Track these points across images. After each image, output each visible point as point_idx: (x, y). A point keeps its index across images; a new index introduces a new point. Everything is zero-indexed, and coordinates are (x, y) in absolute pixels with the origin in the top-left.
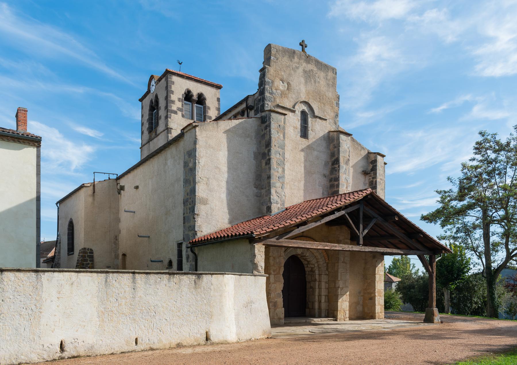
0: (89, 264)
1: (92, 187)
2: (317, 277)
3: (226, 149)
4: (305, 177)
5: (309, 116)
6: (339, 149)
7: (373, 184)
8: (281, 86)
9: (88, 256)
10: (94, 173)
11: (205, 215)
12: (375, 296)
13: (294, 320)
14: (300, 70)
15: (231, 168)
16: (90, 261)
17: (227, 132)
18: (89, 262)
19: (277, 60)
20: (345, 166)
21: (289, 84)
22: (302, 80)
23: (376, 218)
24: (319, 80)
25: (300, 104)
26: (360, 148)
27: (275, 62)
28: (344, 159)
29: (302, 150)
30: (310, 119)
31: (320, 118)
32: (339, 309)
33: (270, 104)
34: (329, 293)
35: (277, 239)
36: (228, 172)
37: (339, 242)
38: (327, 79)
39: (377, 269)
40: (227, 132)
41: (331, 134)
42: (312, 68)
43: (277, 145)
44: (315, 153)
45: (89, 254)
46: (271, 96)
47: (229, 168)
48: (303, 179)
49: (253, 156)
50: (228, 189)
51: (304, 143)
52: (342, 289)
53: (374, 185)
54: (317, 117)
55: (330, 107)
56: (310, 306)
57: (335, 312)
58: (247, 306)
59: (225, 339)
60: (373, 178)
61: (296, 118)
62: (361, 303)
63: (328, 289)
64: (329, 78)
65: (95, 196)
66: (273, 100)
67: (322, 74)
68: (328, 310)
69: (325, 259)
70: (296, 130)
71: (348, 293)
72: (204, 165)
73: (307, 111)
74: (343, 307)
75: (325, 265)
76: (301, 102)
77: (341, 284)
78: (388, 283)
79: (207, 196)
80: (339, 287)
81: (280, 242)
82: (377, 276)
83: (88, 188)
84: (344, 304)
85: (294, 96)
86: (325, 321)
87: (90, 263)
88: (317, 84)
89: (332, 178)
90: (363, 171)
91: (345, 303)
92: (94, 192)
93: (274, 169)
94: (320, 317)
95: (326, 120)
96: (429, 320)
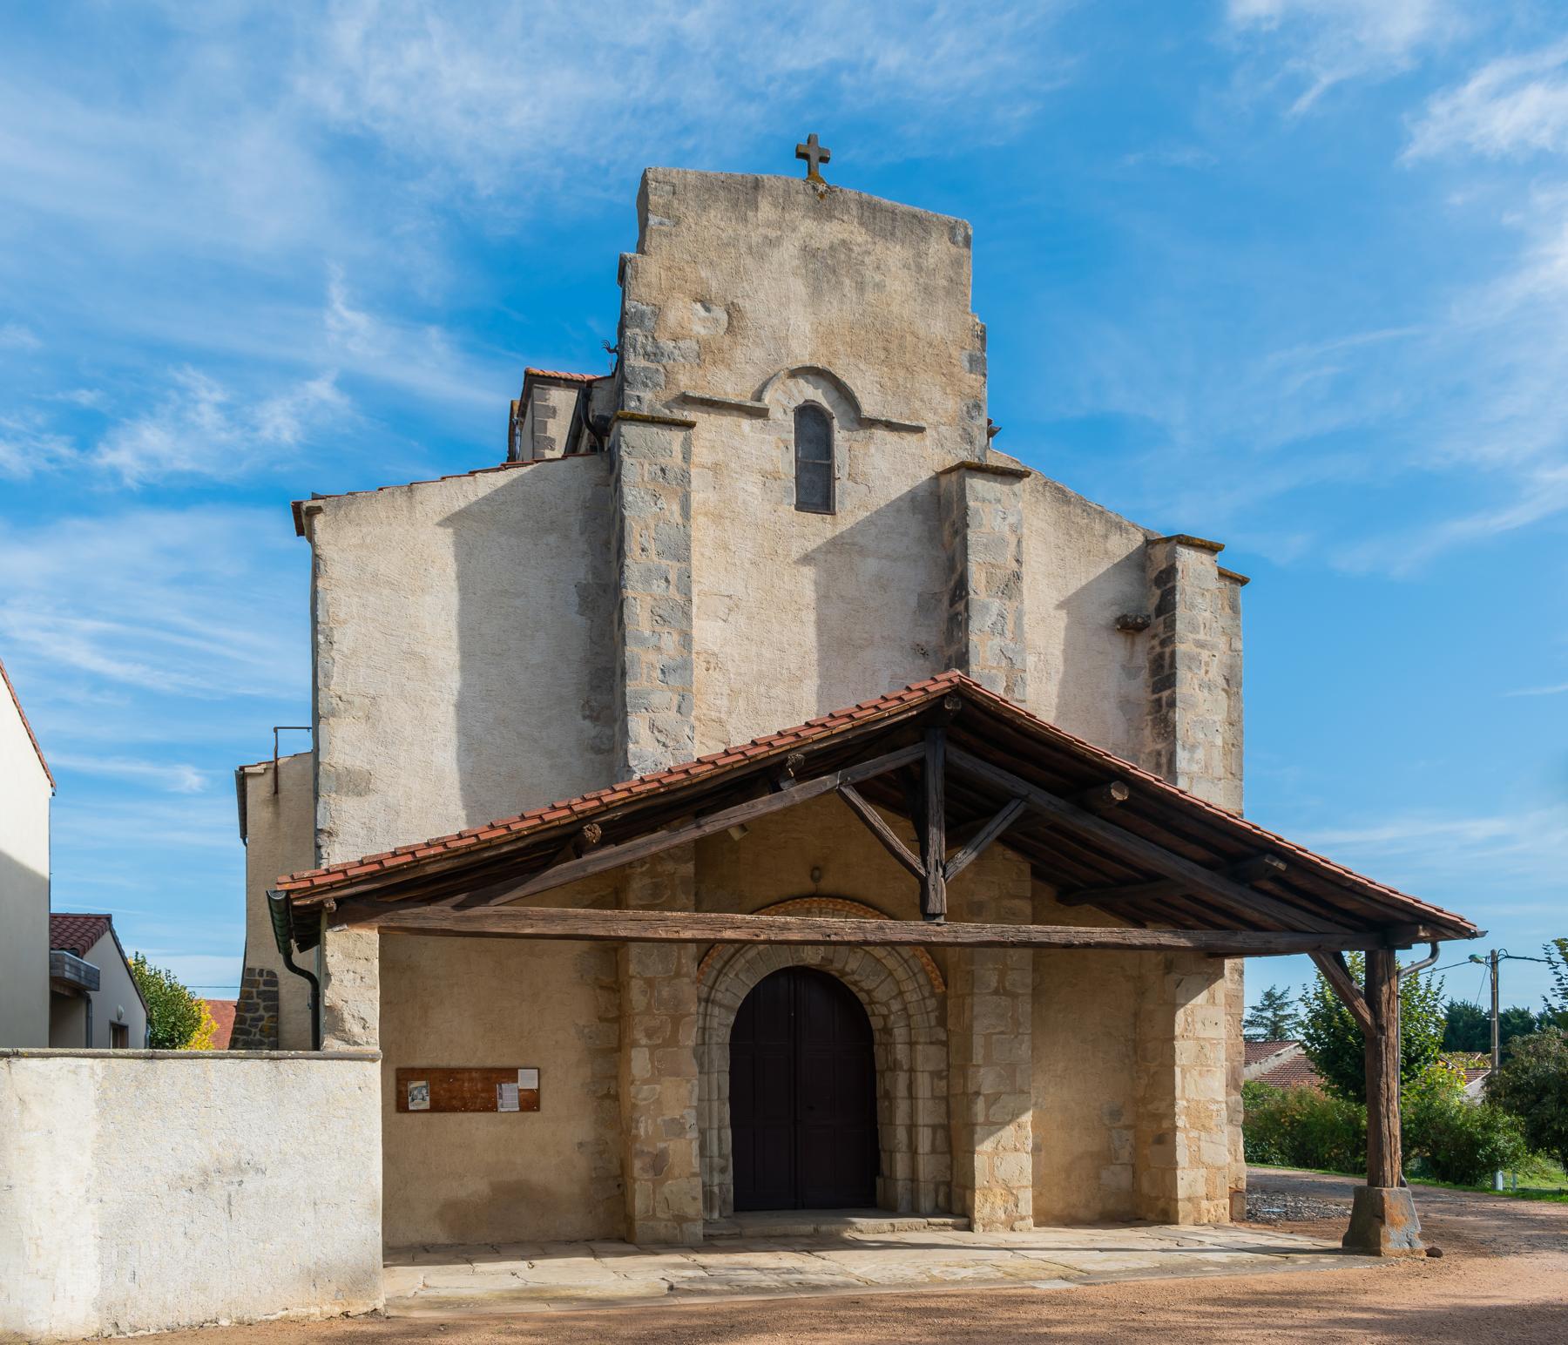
0: (261, 1019)
1: (270, 776)
2: (901, 1052)
3: (454, 584)
4: (821, 662)
5: (835, 422)
6: (965, 538)
7: (1162, 666)
8: (686, 317)
9: (259, 993)
10: (276, 730)
11: (363, 833)
12: (1175, 1128)
14: (788, 251)
15: (475, 648)
16: (266, 1009)
17: (453, 520)
18: (261, 1012)
19: (677, 223)
20: (996, 605)
21: (733, 311)
22: (799, 288)
23: (1023, 798)
24: (878, 278)
25: (790, 383)
26: (1099, 527)
27: (668, 235)
28: (990, 576)
29: (806, 559)
30: (840, 436)
31: (890, 426)
32: (980, 1180)
33: (647, 395)
34: (949, 1114)
36: (463, 668)
38: (920, 268)
39: (1180, 1015)
40: (453, 520)
41: (944, 480)
42: (846, 236)
43: (652, 548)
44: (871, 565)
45: (262, 988)
47: (466, 654)
48: (813, 671)
49: (575, 599)
50: (464, 732)
51: (817, 530)
52: (992, 1100)
53: (1167, 671)
56: (886, 1173)
57: (968, 1192)
58: (204, 1185)
59: (14, 1326)
60: (1163, 643)
61: (772, 438)
62: (1125, 1154)
63: (946, 1099)
64: (931, 262)
65: (282, 803)
66: (662, 379)
67: (895, 254)
68: (949, 1184)
69: (930, 981)
70: (775, 485)
71: (1027, 1118)
72: (354, 652)
74: (1001, 1173)
75: (932, 1003)
76: (794, 374)
77: (986, 1079)
79: (370, 762)
80: (978, 1093)
81: (469, 919)
82: (1178, 1044)
83: (260, 779)
84: (1006, 1160)
85: (758, 354)
86: (911, 1229)
87: (266, 1015)
88: (870, 296)
89: (950, 658)
90: (1118, 620)
91: (1011, 1157)
92: (276, 792)
93: (641, 641)
94: (915, 1212)
96: (1362, 1238)
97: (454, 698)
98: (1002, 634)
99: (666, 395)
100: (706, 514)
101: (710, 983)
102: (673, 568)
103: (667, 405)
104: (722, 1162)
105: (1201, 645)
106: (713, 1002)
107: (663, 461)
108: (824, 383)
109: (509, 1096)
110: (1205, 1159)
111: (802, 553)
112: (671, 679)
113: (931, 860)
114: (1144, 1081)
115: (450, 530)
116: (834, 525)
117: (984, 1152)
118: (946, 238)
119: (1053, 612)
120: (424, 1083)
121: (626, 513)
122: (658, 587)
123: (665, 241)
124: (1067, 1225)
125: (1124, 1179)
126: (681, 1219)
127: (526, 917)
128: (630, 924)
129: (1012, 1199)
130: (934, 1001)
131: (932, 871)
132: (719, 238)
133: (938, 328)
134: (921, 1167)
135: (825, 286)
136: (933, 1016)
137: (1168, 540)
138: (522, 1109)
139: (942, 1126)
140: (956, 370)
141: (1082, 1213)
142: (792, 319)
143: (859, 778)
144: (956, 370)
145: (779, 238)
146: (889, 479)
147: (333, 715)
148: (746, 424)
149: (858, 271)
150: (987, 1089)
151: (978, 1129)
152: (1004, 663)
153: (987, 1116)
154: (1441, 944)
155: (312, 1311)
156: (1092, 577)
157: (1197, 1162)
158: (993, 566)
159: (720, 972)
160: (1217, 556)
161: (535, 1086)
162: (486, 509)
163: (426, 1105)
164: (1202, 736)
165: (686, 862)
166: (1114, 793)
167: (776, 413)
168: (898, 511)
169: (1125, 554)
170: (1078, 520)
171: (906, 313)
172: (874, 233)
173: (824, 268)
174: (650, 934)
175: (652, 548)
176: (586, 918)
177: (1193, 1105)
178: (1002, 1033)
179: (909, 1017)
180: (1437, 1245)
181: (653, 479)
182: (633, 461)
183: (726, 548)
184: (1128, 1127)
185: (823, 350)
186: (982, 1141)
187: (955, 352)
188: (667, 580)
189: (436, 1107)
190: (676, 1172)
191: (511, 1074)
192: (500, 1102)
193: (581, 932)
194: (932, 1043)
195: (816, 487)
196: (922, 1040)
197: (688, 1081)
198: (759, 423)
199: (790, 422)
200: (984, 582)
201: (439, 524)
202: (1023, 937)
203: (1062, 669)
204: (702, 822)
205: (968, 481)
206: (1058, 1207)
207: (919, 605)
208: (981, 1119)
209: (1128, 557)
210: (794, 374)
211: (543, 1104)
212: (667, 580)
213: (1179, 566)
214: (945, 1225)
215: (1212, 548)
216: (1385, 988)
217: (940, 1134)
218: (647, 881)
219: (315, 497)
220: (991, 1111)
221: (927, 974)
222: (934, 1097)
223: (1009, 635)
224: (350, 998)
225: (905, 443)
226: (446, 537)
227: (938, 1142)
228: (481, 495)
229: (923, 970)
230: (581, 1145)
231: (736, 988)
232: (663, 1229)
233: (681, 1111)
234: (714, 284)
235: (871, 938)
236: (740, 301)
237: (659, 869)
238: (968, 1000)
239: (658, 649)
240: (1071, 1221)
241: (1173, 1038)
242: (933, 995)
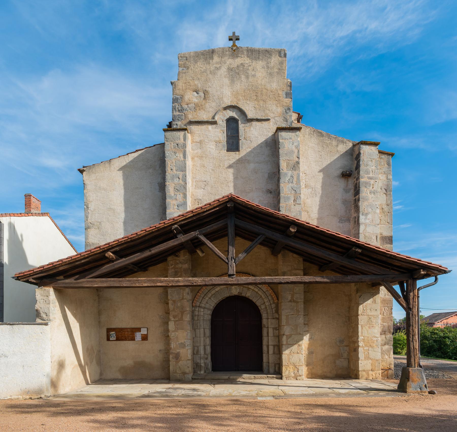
3: (122, 187)
5: (240, 122)
7: (356, 187)
12: (359, 346)
13: (225, 376)
20: (290, 173)
21: (206, 93)
22: (226, 81)
25: (224, 112)
27: (185, 73)
29: (230, 167)
31: (258, 120)
35: (76, 279)
37: (284, 274)
38: (268, 67)
39: (361, 307)
42: (242, 62)
43: (174, 169)
44: (252, 166)
46: (181, 114)
49: (157, 187)
51: (234, 156)
52: (289, 337)
54: (252, 120)
55: (275, 102)
62: (345, 355)
66: (183, 117)
67: (259, 65)
69: (273, 299)
72: (94, 210)
73: (236, 117)
75: (273, 306)
76: (225, 109)
77: (286, 330)
78: (200, 325)
79: (99, 241)
80: (284, 335)
81: (78, 283)
82: (359, 317)
84: (297, 355)
85: (214, 104)
86: (261, 378)
88: (251, 79)
93: (171, 197)
95: (268, 120)
97: (123, 220)
98: (292, 182)
99: (185, 122)
100: (197, 157)
101: (200, 301)
102: (181, 174)
103: (185, 125)
104: (206, 356)
105: (371, 178)
106: (201, 307)
107: (177, 142)
108: (235, 110)
109: (138, 336)
110: (371, 357)
111: (228, 165)
112: (180, 208)
113: (230, 257)
114: (351, 330)
115: (121, 172)
116: (239, 154)
117: (286, 354)
118: (277, 56)
119: (317, 174)
120: (114, 332)
121: (166, 159)
122: (176, 181)
123: (184, 75)
124: (323, 379)
125: (345, 364)
126: (184, 373)
127: (95, 281)
128: (127, 282)
129: (296, 369)
130: (274, 305)
131: (230, 260)
132: (201, 70)
133: (274, 86)
134: (270, 359)
135: (235, 79)
136: (274, 310)
137: (358, 143)
138: (142, 340)
139: (277, 345)
140: (281, 98)
141: (329, 375)
142: (224, 91)
143: (204, 232)
144: (281, 98)
145: (220, 67)
146: (258, 137)
147: (89, 228)
148: (210, 127)
149: (246, 72)
150: (287, 333)
151: (284, 346)
152: (293, 192)
153: (287, 342)
154: (438, 276)
155: (20, 397)
156: (332, 160)
157: (367, 357)
158: (289, 160)
159: (203, 298)
160: (378, 147)
161: (146, 333)
162: (131, 164)
163: (115, 339)
164: (370, 210)
165: (185, 264)
166: (291, 229)
167: (220, 122)
168: (261, 147)
169: (345, 150)
170: (327, 141)
171: (263, 83)
172: (252, 59)
173: (234, 74)
174: (134, 285)
175: (174, 169)
176: (113, 281)
177: (366, 338)
178: (293, 314)
180: (433, 389)
181: (174, 148)
182: (168, 143)
183: (204, 166)
184: (347, 346)
185: (235, 100)
186: (285, 350)
187: (280, 92)
188: (179, 178)
189: (118, 339)
190: (183, 359)
191: (139, 330)
192: (136, 338)
193: (112, 285)
194: (273, 318)
195: (233, 143)
196: (270, 317)
197: (186, 331)
198: (214, 126)
199: (224, 124)
200: (285, 166)
201: (118, 170)
202: (263, 281)
203: (321, 192)
204: (151, 249)
205: (280, 133)
206: (320, 372)
207: (269, 177)
208: (284, 343)
209: (346, 152)
210: (225, 109)
211: (149, 338)
212: (179, 178)
213: (362, 152)
214: (273, 377)
215: (376, 144)
216: (411, 294)
217: (276, 348)
218: (173, 270)
219: (84, 167)
220: (289, 340)
221: (272, 296)
222: (274, 336)
223: (295, 182)
224: (42, 307)
225: (263, 125)
226: (120, 173)
227: (275, 351)
228: (130, 160)
229: (270, 295)
230: (160, 350)
231: (210, 303)
232: (178, 376)
233: (189, 340)
234: (199, 85)
235: (207, 283)
236: (207, 89)
237: (177, 266)
239: (176, 199)
240: (324, 377)
241: (358, 315)
242: (274, 303)
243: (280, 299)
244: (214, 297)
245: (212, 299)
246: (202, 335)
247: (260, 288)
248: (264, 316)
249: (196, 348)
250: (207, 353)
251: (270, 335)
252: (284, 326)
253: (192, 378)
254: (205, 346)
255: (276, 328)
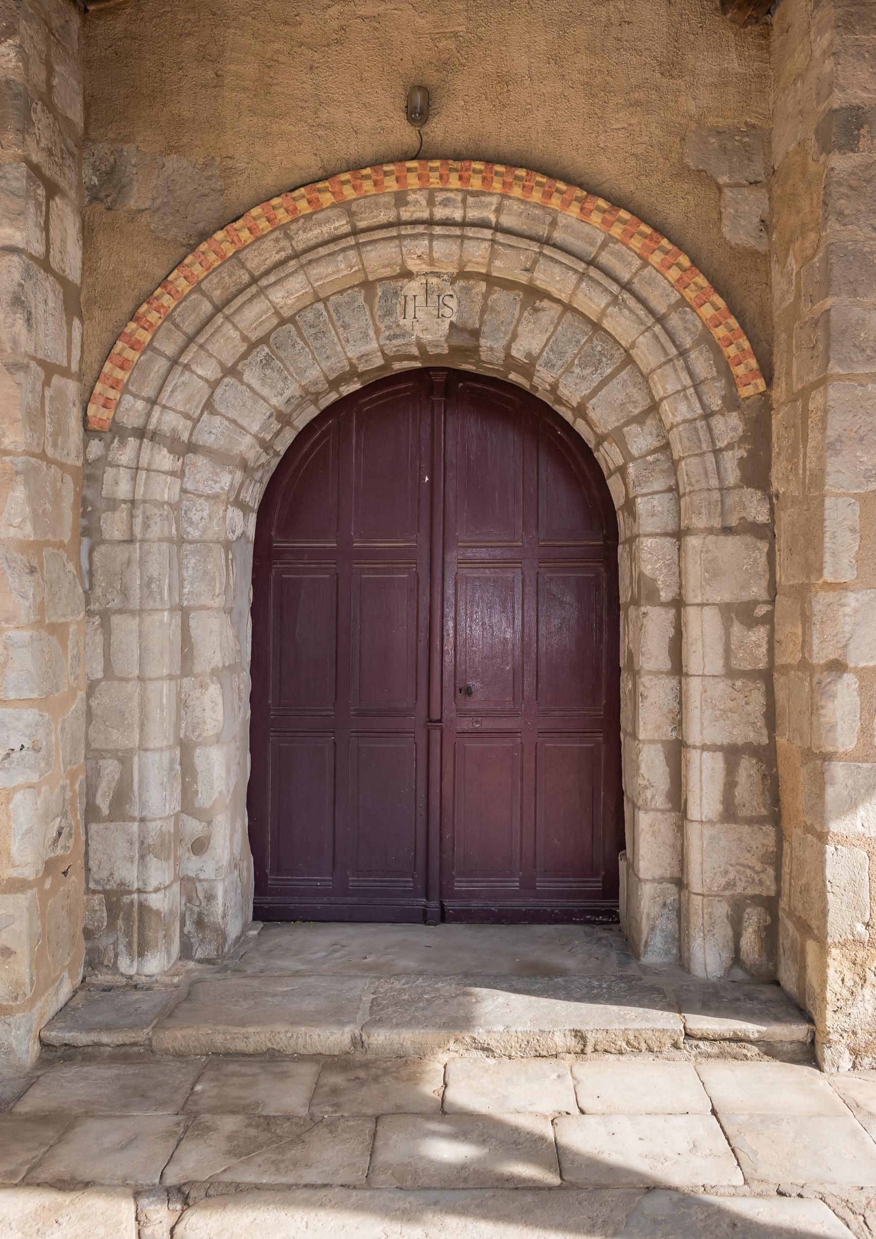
63: (767, 677)
68: (770, 904)
69: (724, 369)
75: (729, 426)
78: (147, 584)
80: (837, 667)
101: (149, 391)
106: (155, 436)
134: (695, 857)
136: (731, 461)
151: (838, 770)
159: (174, 362)
179: (675, 464)
186: (851, 805)
194: (727, 530)
196: (700, 522)
217: (748, 770)
221: (716, 349)
222: (731, 673)
227: (742, 793)
229: (706, 339)
238: (816, 401)
242: (732, 403)
243: (793, 370)
244: (267, 362)
245: (251, 376)
246: (163, 664)
247: (626, 287)
248: (647, 513)
249: (110, 768)
250: (205, 797)
251: (694, 662)
252: (842, 587)
253: (45, 1045)
254: (186, 749)
255: (754, 603)
